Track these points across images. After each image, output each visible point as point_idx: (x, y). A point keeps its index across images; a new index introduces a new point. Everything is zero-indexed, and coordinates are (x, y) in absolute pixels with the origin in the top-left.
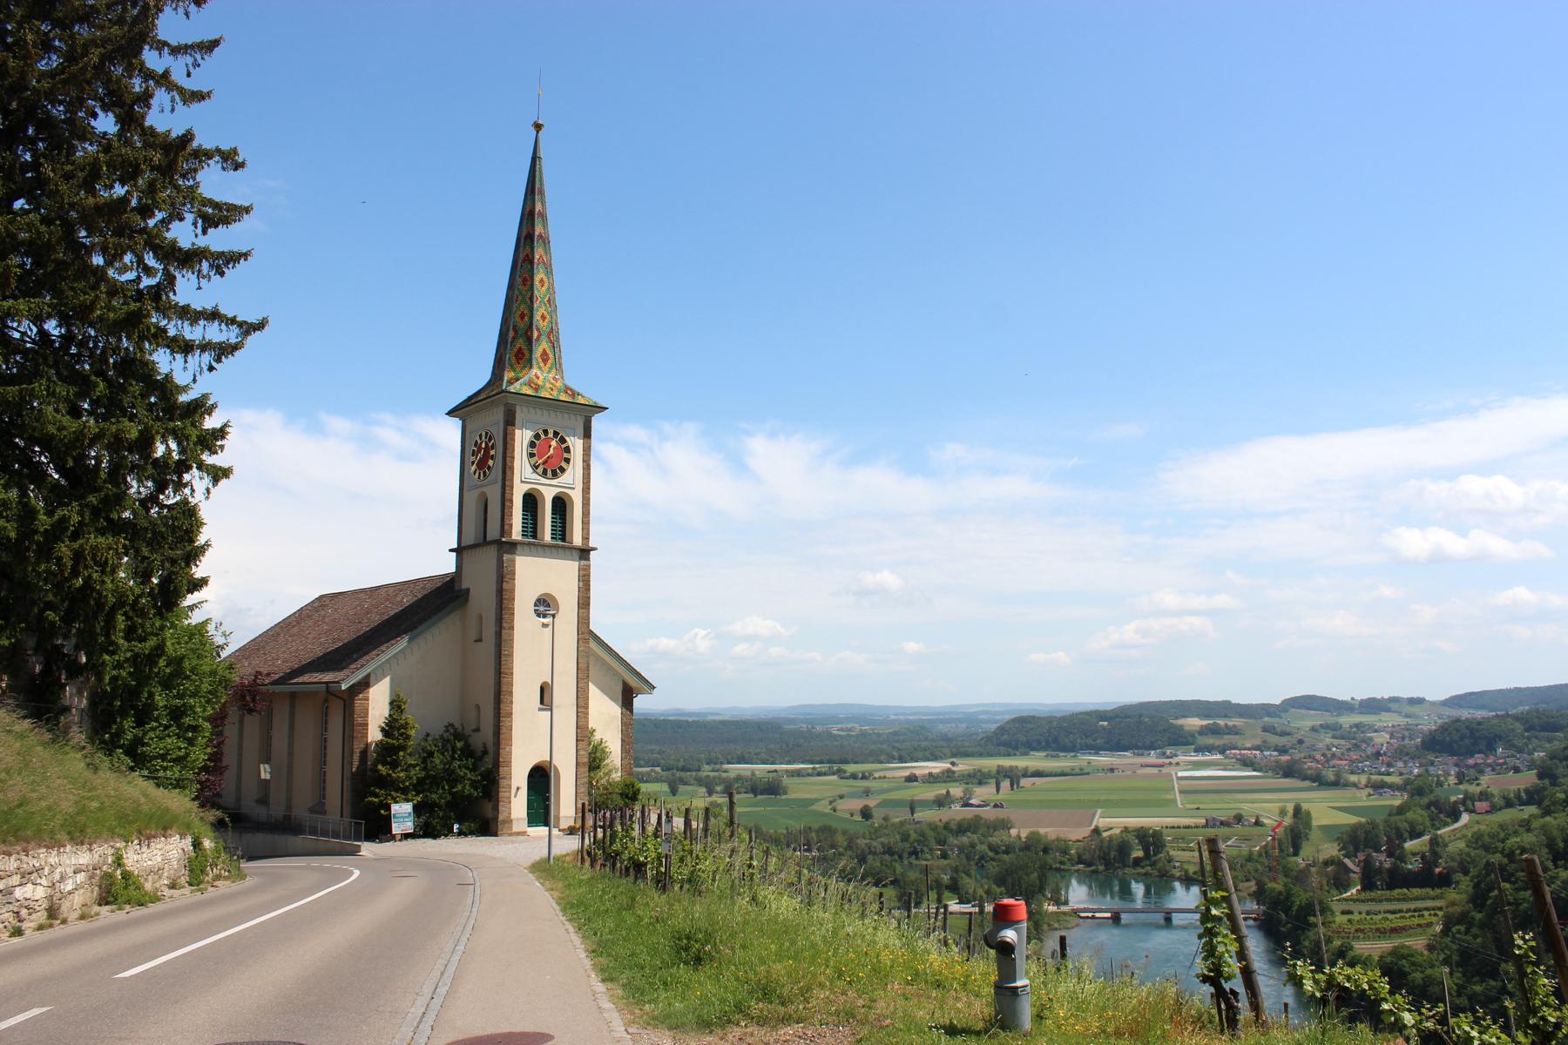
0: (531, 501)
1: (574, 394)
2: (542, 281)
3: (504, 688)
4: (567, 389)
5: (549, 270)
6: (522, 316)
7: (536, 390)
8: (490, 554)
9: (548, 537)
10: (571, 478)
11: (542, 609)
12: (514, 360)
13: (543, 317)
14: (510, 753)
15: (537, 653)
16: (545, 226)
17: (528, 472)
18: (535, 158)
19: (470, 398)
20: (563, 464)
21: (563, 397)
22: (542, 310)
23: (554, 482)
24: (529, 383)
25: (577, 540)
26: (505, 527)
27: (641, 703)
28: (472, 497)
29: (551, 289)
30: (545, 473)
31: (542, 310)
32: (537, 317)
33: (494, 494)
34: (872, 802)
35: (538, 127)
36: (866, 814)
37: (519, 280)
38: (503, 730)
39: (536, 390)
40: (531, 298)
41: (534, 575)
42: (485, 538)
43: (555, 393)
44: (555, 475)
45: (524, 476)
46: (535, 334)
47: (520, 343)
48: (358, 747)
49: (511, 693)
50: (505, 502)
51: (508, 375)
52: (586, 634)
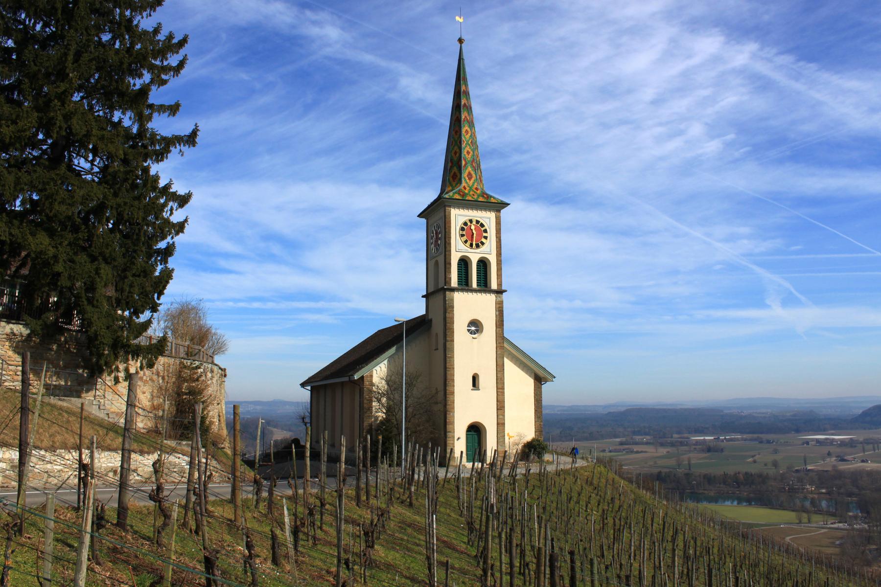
0: (464, 263)
1: (489, 197)
2: (470, 175)
3: (448, 377)
4: (484, 194)
5: (471, 124)
6: (455, 153)
7: (463, 196)
8: (439, 297)
9: (475, 285)
10: (489, 250)
11: (473, 328)
12: (451, 179)
13: (468, 153)
14: (454, 416)
15: (471, 355)
16: (466, 85)
17: (461, 246)
18: (461, 59)
19: (429, 207)
20: (483, 240)
21: (481, 199)
22: (468, 149)
23: (478, 251)
24: (459, 192)
25: (494, 286)
26: (447, 280)
27: (546, 387)
28: (432, 263)
29: (473, 136)
30: (471, 245)
31: (468, 149)
32: (464, 152)
33: (441, 259)
34: (778, 457)
35: (461, 41)
36: (775, 464)
37: (453, 133)
38: (449, 403)
39: (463, 196)
40: (460, 142)
41: (467, 306)
42: (437, 292)
43: (475, 197)
44: (478, 246)
45: (458, 249)
46: (463, 163)
47: (455, 169)
48: (366, 424)
49: (453, 341)
50: (447, 264)
51: (447, 189)
52: (500, 338)
